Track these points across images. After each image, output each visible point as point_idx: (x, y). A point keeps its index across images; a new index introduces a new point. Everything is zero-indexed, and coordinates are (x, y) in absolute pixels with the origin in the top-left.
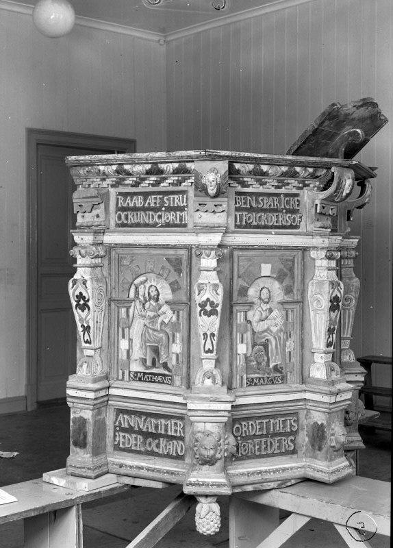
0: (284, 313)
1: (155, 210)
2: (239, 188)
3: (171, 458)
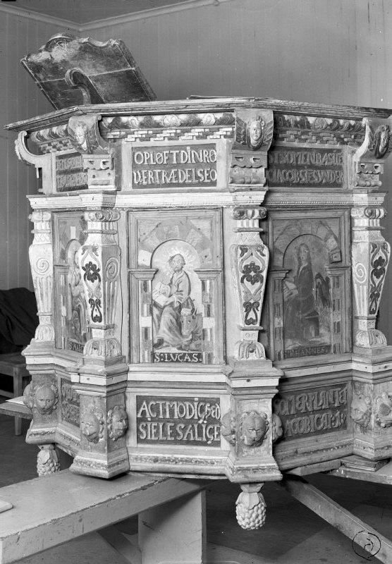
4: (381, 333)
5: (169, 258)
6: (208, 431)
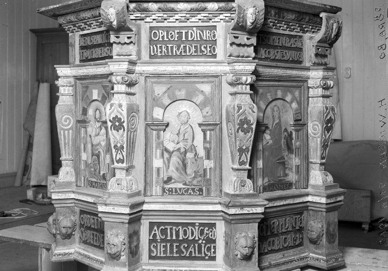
3: (89, 245)
4: (329, 174)
5: (178, 114)
6: (206, 249)
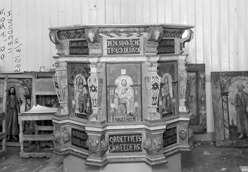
0: (133, 90)
1: (80, 48)
2: (109, 38)
